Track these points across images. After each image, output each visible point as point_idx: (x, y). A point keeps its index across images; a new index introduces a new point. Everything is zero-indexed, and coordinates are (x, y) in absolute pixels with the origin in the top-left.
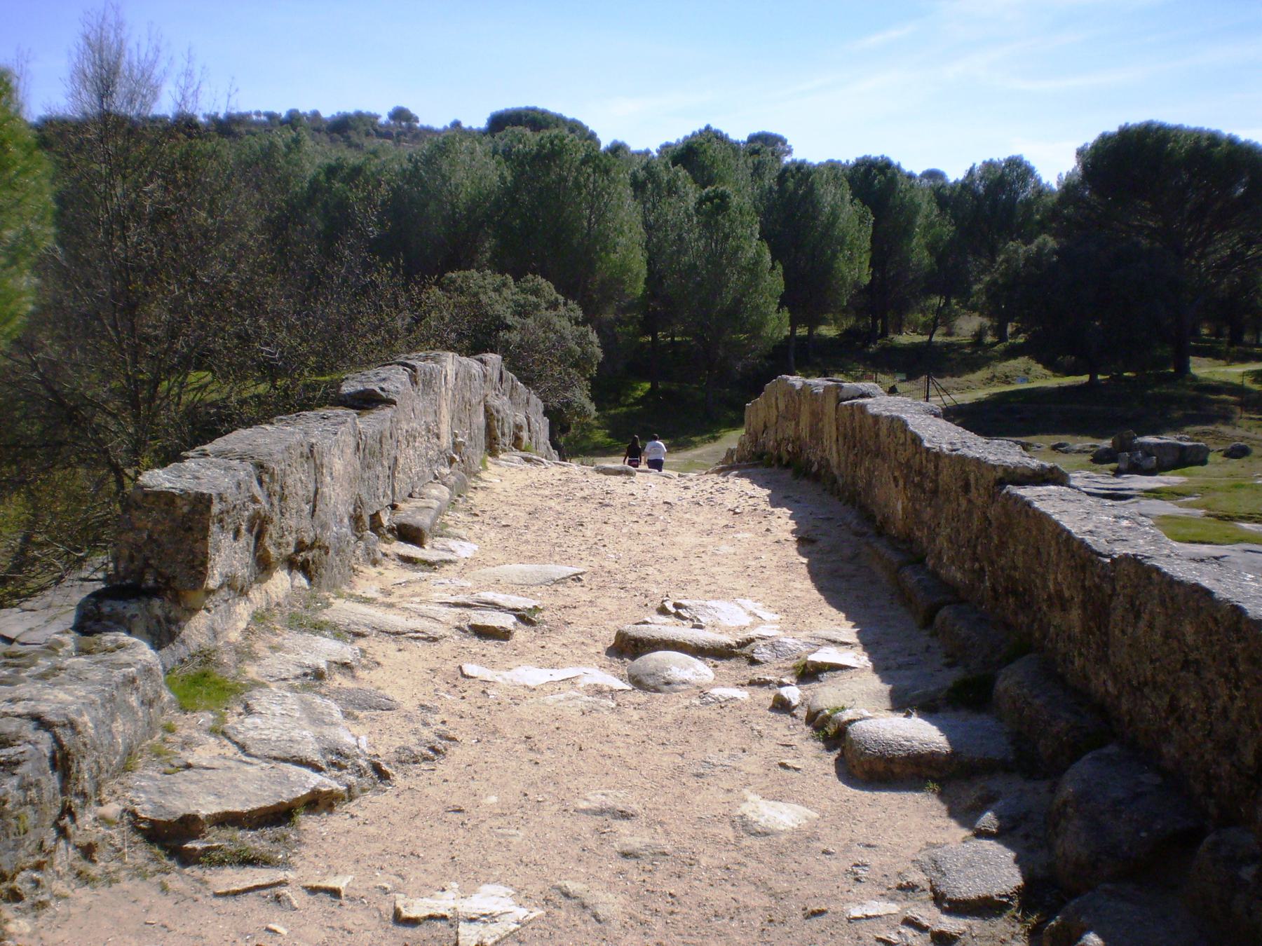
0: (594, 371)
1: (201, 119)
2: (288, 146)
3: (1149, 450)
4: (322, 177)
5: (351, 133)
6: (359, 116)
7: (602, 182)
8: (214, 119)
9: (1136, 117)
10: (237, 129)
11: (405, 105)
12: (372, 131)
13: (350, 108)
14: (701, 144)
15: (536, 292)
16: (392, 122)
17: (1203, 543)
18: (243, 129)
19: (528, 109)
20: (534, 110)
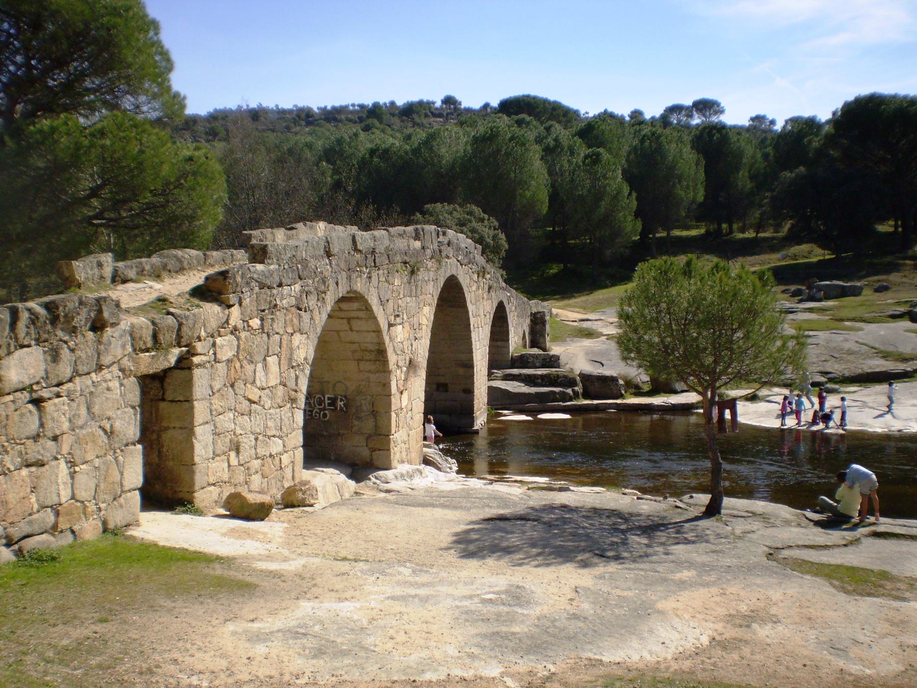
0: (503, 254)
1: (316, 110)
2: (350, 138)
3: (820, 289)
4: (367, 156)
5: (415, 116)
6: (421, 103)
7: (519, 150)
8: (324, 110)
9: (865, 90)
10: (338, 117)
11: (452, 94)
12: (429, 114)
13: (415, 98)
14: (597, 122)
15: (470, 213)
16: (444, 106)
17: (812, 330)
18: (343, 117)
19: (524, 96)
20: (528, 96)
